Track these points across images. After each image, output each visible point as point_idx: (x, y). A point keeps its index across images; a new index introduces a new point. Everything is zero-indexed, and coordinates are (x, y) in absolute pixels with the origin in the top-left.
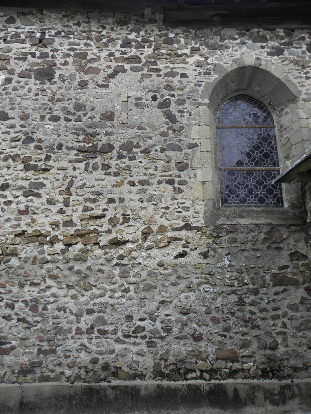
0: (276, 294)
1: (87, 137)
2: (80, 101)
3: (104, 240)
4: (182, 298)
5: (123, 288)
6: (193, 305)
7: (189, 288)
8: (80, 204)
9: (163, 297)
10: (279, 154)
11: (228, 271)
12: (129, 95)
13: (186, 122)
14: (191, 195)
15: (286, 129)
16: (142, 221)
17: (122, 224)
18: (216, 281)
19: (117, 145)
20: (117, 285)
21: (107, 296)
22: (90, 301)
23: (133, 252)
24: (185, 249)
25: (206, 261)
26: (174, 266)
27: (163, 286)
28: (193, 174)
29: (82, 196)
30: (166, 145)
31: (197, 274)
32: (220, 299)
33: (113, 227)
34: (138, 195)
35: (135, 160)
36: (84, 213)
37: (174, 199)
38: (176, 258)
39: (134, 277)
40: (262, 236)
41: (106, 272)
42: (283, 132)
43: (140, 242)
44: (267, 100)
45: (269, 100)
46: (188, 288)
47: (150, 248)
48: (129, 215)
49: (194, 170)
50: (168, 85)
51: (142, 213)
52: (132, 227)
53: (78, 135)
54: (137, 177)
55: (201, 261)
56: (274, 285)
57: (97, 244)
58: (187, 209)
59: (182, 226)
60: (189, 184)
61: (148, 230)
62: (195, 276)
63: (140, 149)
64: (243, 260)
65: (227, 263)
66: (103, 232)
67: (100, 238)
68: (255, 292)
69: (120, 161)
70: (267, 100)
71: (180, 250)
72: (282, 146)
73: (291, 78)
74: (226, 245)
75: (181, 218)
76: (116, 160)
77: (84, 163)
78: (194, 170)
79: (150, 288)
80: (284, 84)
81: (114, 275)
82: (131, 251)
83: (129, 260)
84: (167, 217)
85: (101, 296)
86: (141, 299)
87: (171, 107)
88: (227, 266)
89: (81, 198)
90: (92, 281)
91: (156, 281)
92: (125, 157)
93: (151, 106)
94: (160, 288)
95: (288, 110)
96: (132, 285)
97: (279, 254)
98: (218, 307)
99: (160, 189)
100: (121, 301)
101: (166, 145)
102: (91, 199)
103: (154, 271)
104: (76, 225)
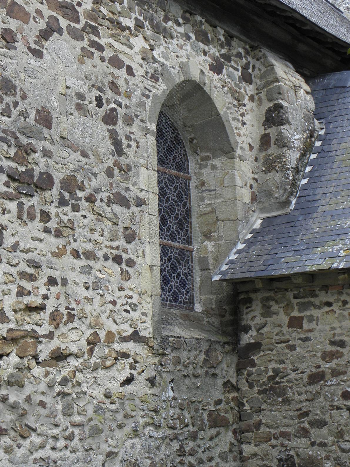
0: (211, 439)
1: (20, 152)
2: (7, 74)
3: (45, 350)
4: (128, 447)
5: (67, 433)
6: (139, 458)
7: (136, 433)
8: (13, 282)
9: (110, 446)
10: (193, 226)
11: (171, 407)
12: (69, 84)
13: (132, 158)
14: (139, 285)
15: (210, 191)
16: (87, 322)
17: (66, 324)
18: (160, 420)
19: (57, 177)
20: (60, 429)
21: (48, 447)
22: (28, 456)
23: (77, 374)
24: (133, 372)
25: (152, 391)
26: (122, 398)
27: (111, 429)
28: (141, 251)
29: (15, 266)
30: (113, 194)
31: (144, 410)
32: (163, 448)
33: (56, 328)
34: (82, 276)
35: (78, 212)
36: (20, 299)
37: (121, 289)
38: (123, 384)
39: (79, 414)
40: (203, 357)
41: (48, 406)
42: (205, 194)
43: (86, 357)
44: (190, 135)
45: (193, 136)
46: (134, 431)
47: (95, 369)
48: (73, 309)
49: (143, 244)
50: (113, 83)
51: (88, 308)
52: (76, 330)
53: (9, 146)
54: (82, 244)
55: (147, 391)
56: (211, 427)
57: (35, 357)
58: (134, 307)
59: (131, 335)
60: (137, 266)
61: (95, 338)
62: (142, 413)
63: (84, 193)
64: (184, 390)
65: (171, 394)
66: (44, 336)
67: (40, 347)
68: (194, 437)
69: (61, 209)
70: (190, 135)
71: (127, 373)
72: (201, 215)
73: (230, 117)
74: (171, 367)
75: (129, 322)
76: (56, 207)
77: (16, 203)
78: (143, 244)
79: (96, 432)
80: (223, 124)
81: (56, 410)
82: (75, 372)
83: (73, 386)
84: (116, 318)
85: (42, 447)
86: (87, 450)
87: (117, 126)
88: (170, 399)
89: (14, 271)
90: (31, 421)
91: (103, 421)
92: (68, 205)
93: (96, 115)
94: (106, 432)
95: (217, 162)
96: (76, 428)
97: (214, 383)
98: (162, 459)
99: (106, 270)
100: (64, 455)
101: (113, 194)
102: (27, 273)
103: (101, 404)
104: (8, 320)
